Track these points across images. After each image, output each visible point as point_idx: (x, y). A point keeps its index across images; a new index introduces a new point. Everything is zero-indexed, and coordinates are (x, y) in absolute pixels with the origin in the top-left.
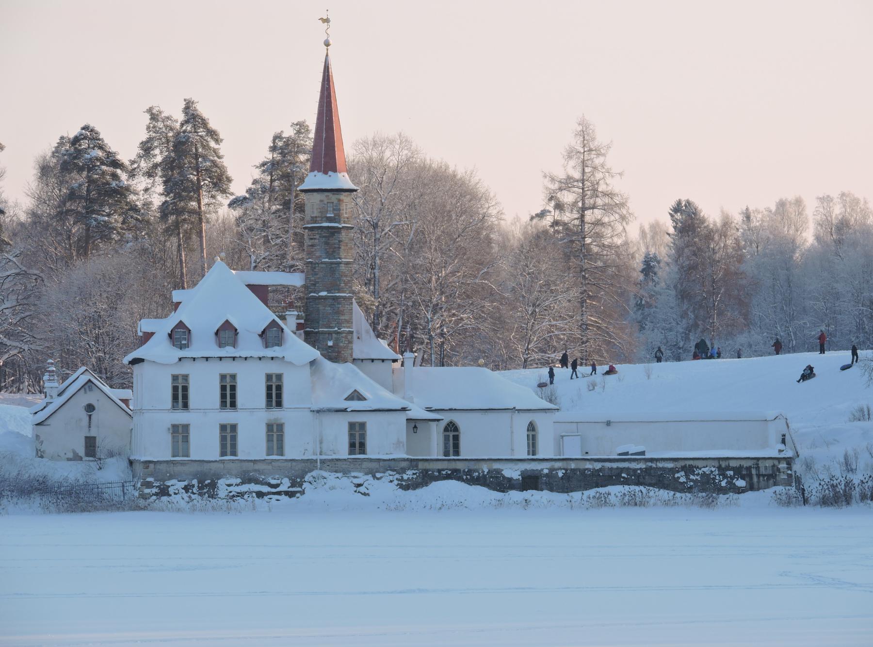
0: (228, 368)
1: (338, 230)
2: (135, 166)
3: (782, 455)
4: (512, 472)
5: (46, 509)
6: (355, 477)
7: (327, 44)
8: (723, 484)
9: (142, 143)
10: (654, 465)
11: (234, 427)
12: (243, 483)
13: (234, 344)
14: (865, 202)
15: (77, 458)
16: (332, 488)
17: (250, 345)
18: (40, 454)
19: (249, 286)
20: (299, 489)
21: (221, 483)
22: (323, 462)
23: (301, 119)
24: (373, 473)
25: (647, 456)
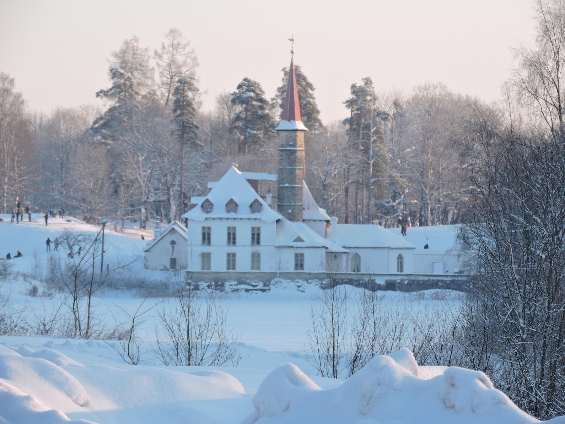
0: (231, 224)
2: (274, 101)
4: (381, 281)
5: (134, 297)
6: (297, 282)
7: (292, 52)
9: (279, 88)
10: (456, 279)
11: (234, 255)
12: (238, 284)
15: (165, 269)
17: (244, 212)
18: (146, 267)
21: (227, 284)
22: (280, 274)
23: (368, 76)
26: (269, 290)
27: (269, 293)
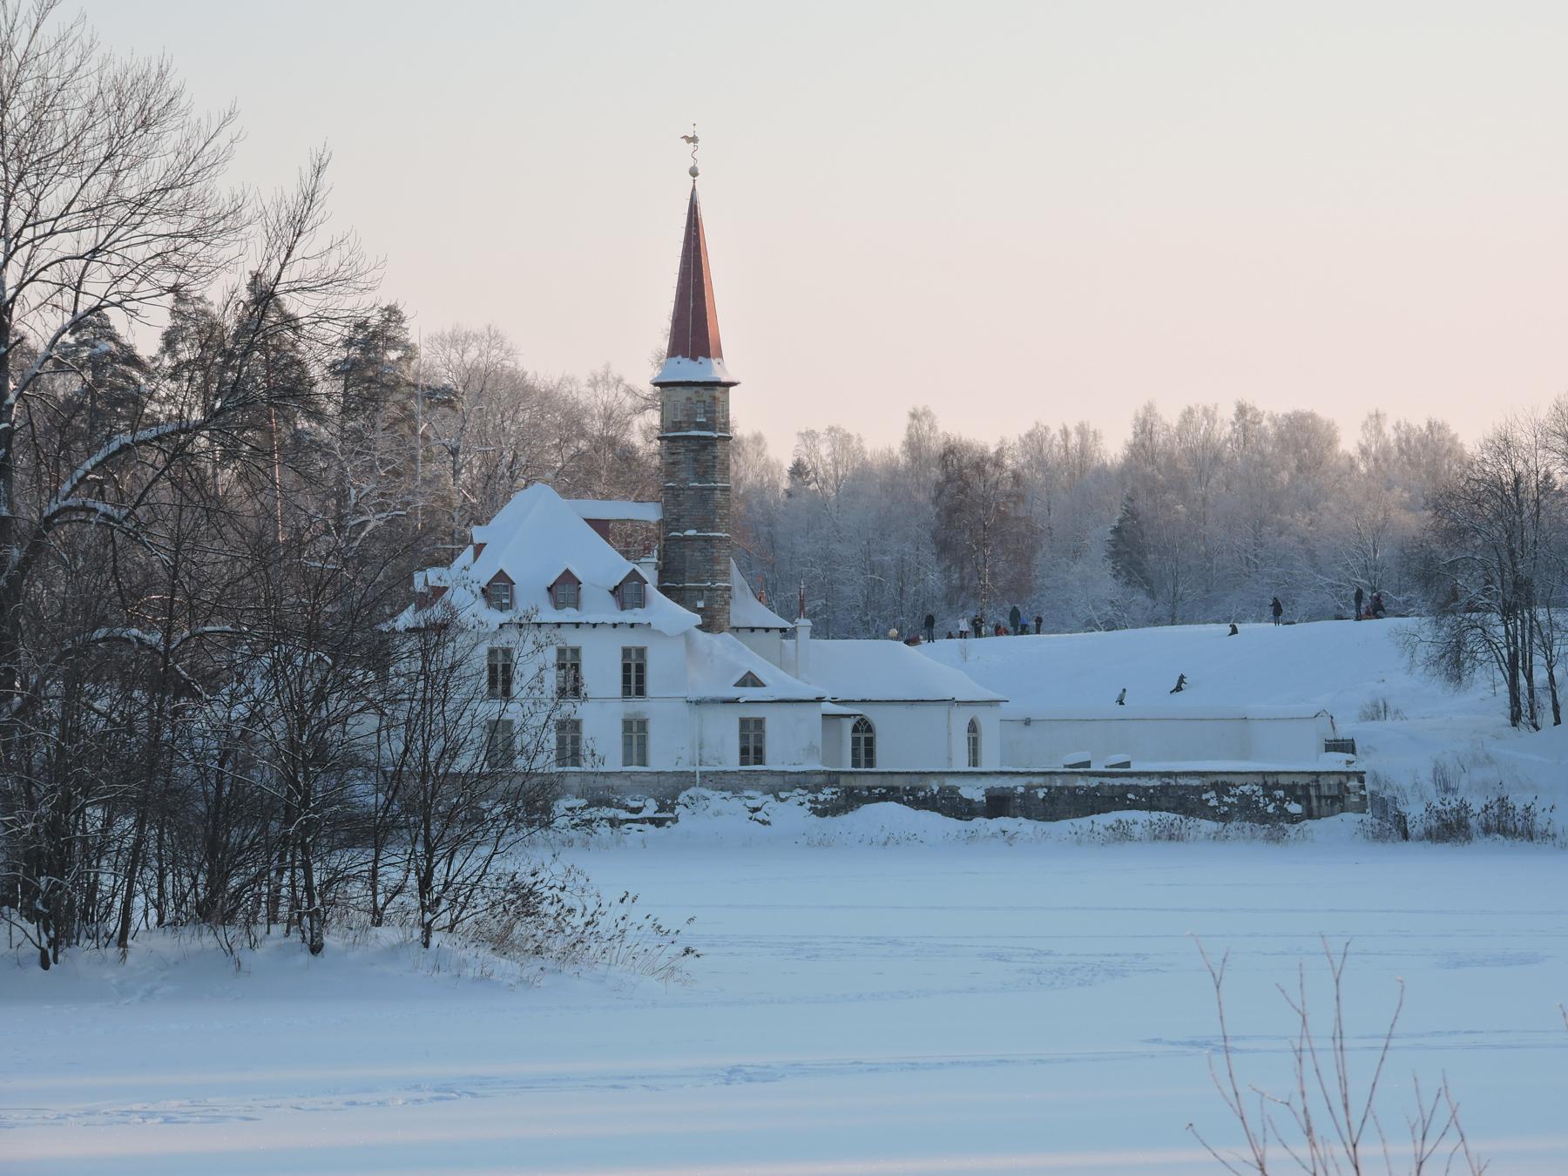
1: (711, 442)
3: (1351, 769)
4: (973, 791)
7: (694, 173)
8: (1270, 809)
12: (589, 806)
13: (576, 605)
14: (860, 440)
16: (726, 811)
19: (587, 520)
20: (670, 815)
22: (704, 775)
24: (774, 792)
25: (1133, 768)
26: (675, 820)
27: (674, 827)
